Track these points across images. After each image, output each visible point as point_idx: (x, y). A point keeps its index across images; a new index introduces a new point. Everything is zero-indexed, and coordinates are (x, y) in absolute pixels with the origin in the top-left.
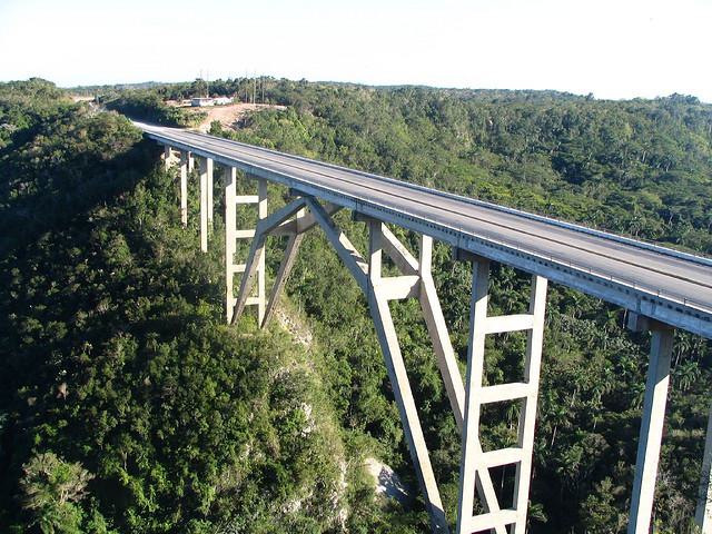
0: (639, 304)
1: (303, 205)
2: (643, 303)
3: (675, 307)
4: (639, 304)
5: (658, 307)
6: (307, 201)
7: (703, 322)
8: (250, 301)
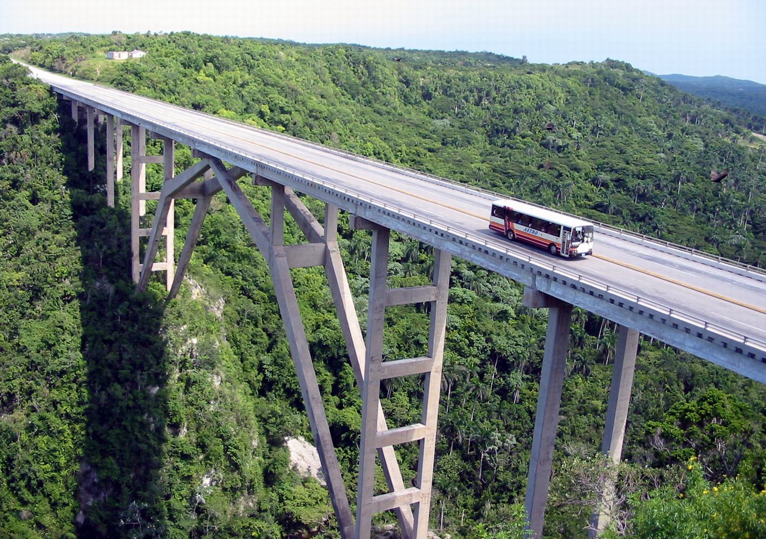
0: (534, 279)
1: (208, 167)
2: (538, 278)
3: (746, 352)
4: (534, 279)
5: (553, 283)
6: (211, 163)
7: (598, 300)
8: (156, 267)
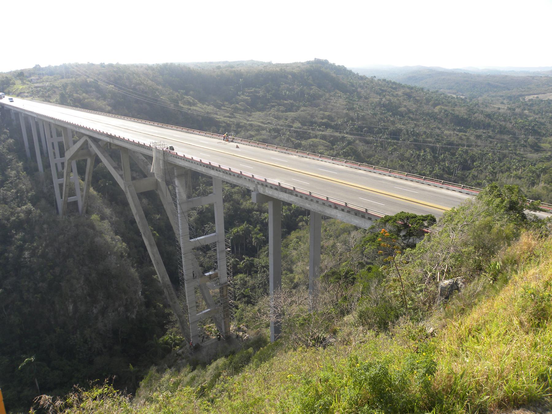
8: (71, 199)
